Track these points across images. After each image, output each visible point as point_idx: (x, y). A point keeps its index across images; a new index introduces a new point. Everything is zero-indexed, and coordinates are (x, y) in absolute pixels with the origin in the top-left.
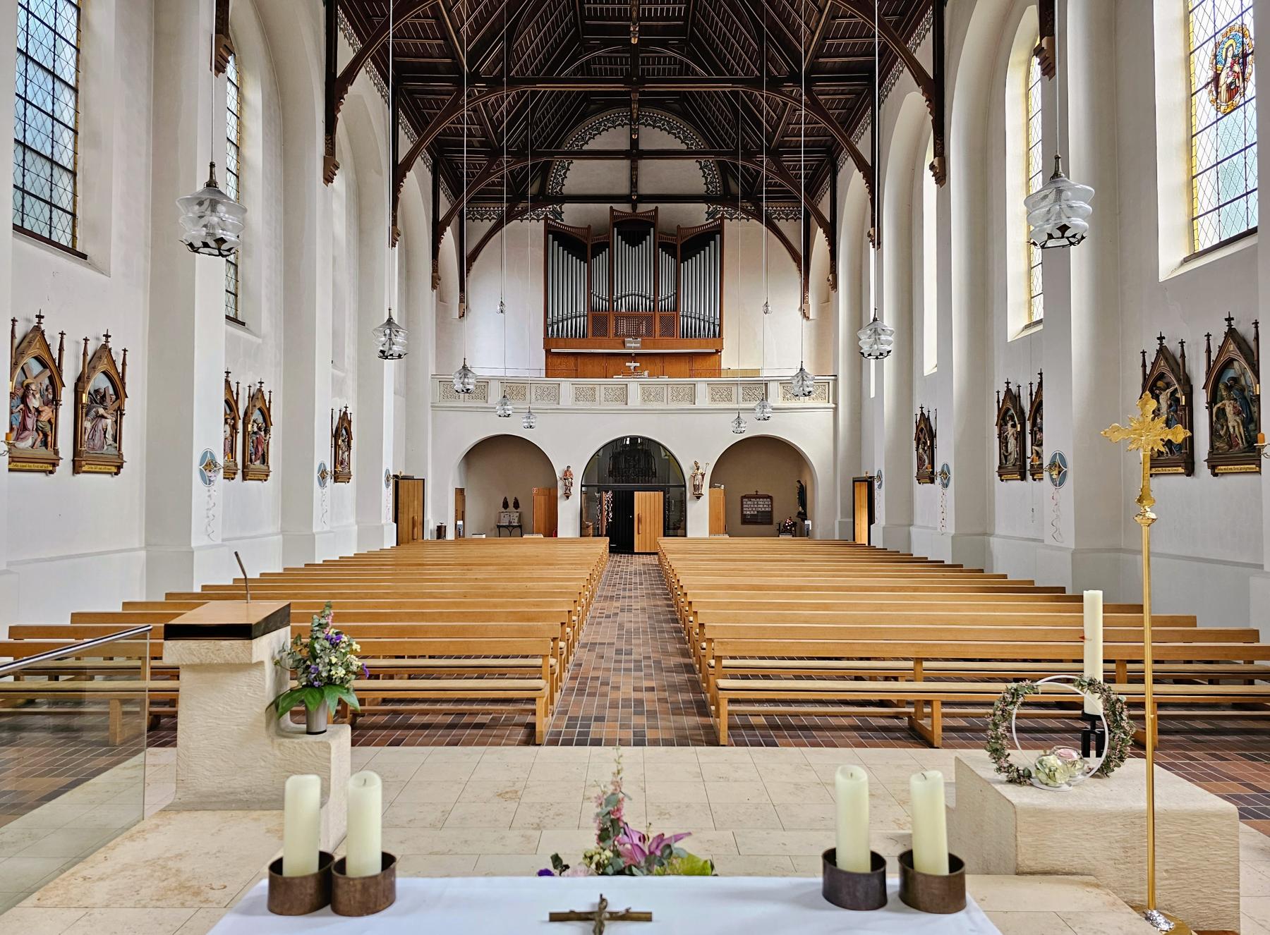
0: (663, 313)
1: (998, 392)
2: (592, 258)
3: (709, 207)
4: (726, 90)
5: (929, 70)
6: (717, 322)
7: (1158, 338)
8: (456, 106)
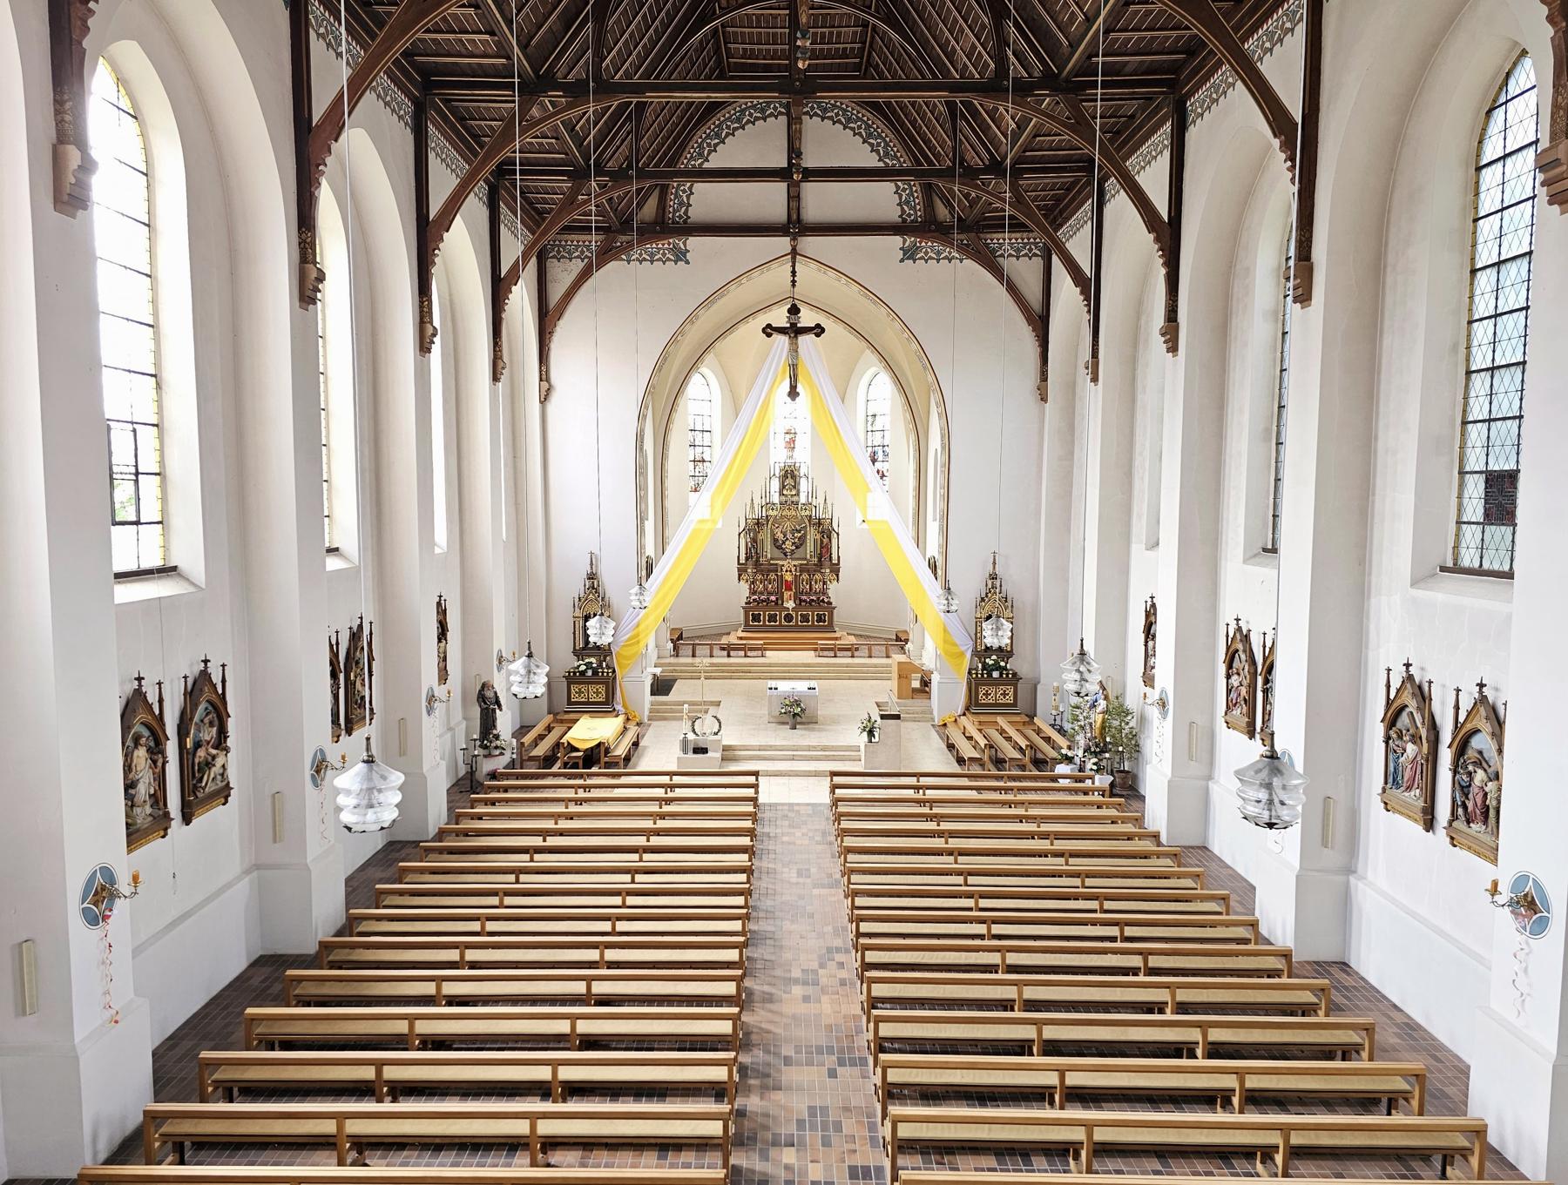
5: (1163, 210)
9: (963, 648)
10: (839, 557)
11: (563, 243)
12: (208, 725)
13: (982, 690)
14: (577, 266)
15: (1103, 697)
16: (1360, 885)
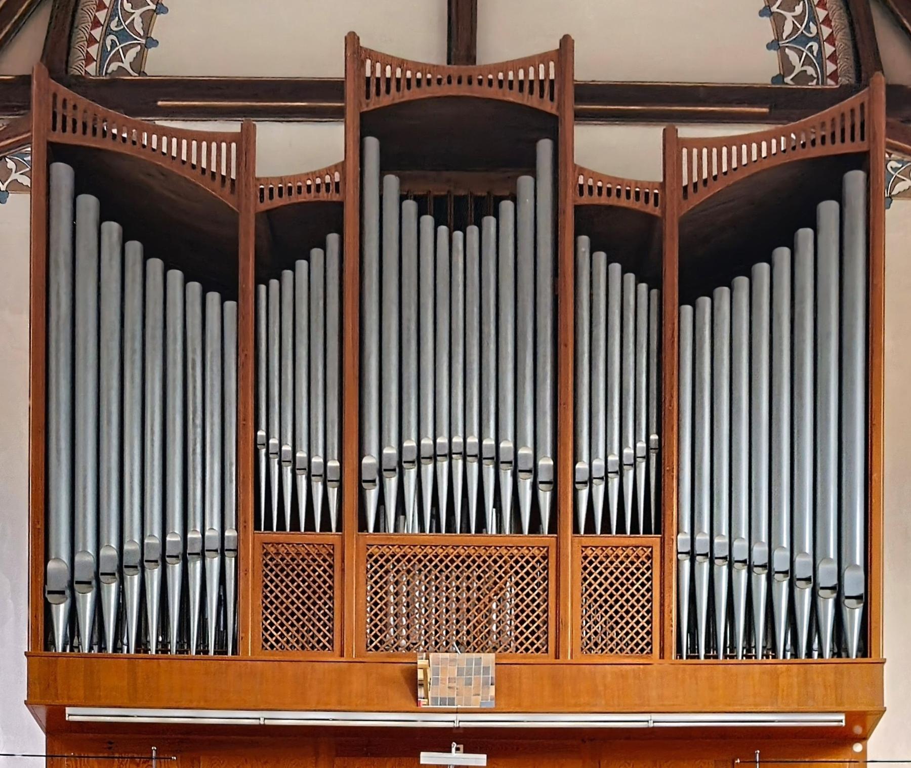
0: (599, 538)
2: (262, 279)
6: (853, 584)
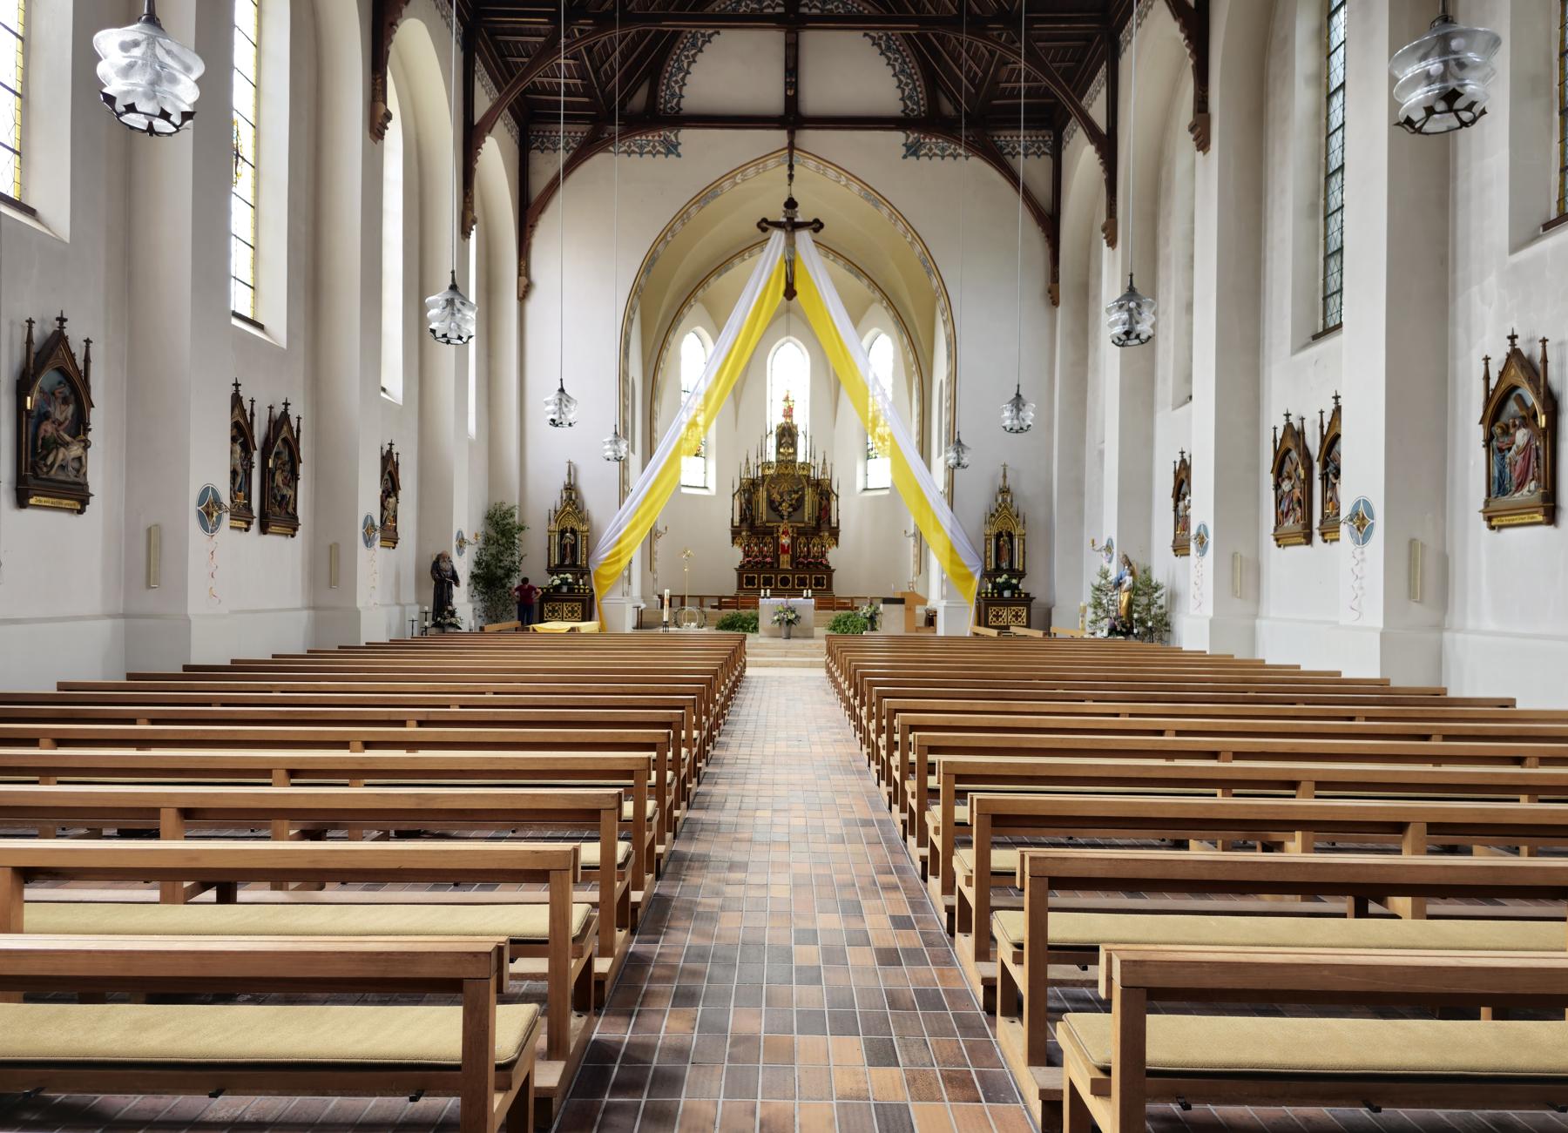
1: (1275, 428)
3: (908, 137)
4: (911, 32)
7: (1509, 337)
8: (551, 48)
9: (972, 570)
10: (838, 520)
11: (547, 134)
12: (60, 401)
13: (993, 610)
14: (562, 157)
15: (1128, 572)
16: (1459, 636)
